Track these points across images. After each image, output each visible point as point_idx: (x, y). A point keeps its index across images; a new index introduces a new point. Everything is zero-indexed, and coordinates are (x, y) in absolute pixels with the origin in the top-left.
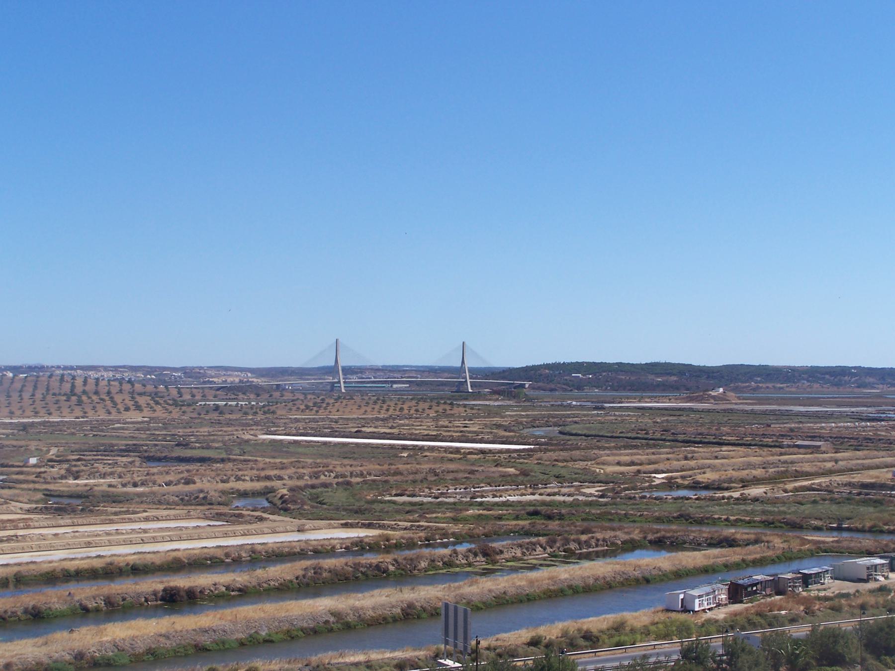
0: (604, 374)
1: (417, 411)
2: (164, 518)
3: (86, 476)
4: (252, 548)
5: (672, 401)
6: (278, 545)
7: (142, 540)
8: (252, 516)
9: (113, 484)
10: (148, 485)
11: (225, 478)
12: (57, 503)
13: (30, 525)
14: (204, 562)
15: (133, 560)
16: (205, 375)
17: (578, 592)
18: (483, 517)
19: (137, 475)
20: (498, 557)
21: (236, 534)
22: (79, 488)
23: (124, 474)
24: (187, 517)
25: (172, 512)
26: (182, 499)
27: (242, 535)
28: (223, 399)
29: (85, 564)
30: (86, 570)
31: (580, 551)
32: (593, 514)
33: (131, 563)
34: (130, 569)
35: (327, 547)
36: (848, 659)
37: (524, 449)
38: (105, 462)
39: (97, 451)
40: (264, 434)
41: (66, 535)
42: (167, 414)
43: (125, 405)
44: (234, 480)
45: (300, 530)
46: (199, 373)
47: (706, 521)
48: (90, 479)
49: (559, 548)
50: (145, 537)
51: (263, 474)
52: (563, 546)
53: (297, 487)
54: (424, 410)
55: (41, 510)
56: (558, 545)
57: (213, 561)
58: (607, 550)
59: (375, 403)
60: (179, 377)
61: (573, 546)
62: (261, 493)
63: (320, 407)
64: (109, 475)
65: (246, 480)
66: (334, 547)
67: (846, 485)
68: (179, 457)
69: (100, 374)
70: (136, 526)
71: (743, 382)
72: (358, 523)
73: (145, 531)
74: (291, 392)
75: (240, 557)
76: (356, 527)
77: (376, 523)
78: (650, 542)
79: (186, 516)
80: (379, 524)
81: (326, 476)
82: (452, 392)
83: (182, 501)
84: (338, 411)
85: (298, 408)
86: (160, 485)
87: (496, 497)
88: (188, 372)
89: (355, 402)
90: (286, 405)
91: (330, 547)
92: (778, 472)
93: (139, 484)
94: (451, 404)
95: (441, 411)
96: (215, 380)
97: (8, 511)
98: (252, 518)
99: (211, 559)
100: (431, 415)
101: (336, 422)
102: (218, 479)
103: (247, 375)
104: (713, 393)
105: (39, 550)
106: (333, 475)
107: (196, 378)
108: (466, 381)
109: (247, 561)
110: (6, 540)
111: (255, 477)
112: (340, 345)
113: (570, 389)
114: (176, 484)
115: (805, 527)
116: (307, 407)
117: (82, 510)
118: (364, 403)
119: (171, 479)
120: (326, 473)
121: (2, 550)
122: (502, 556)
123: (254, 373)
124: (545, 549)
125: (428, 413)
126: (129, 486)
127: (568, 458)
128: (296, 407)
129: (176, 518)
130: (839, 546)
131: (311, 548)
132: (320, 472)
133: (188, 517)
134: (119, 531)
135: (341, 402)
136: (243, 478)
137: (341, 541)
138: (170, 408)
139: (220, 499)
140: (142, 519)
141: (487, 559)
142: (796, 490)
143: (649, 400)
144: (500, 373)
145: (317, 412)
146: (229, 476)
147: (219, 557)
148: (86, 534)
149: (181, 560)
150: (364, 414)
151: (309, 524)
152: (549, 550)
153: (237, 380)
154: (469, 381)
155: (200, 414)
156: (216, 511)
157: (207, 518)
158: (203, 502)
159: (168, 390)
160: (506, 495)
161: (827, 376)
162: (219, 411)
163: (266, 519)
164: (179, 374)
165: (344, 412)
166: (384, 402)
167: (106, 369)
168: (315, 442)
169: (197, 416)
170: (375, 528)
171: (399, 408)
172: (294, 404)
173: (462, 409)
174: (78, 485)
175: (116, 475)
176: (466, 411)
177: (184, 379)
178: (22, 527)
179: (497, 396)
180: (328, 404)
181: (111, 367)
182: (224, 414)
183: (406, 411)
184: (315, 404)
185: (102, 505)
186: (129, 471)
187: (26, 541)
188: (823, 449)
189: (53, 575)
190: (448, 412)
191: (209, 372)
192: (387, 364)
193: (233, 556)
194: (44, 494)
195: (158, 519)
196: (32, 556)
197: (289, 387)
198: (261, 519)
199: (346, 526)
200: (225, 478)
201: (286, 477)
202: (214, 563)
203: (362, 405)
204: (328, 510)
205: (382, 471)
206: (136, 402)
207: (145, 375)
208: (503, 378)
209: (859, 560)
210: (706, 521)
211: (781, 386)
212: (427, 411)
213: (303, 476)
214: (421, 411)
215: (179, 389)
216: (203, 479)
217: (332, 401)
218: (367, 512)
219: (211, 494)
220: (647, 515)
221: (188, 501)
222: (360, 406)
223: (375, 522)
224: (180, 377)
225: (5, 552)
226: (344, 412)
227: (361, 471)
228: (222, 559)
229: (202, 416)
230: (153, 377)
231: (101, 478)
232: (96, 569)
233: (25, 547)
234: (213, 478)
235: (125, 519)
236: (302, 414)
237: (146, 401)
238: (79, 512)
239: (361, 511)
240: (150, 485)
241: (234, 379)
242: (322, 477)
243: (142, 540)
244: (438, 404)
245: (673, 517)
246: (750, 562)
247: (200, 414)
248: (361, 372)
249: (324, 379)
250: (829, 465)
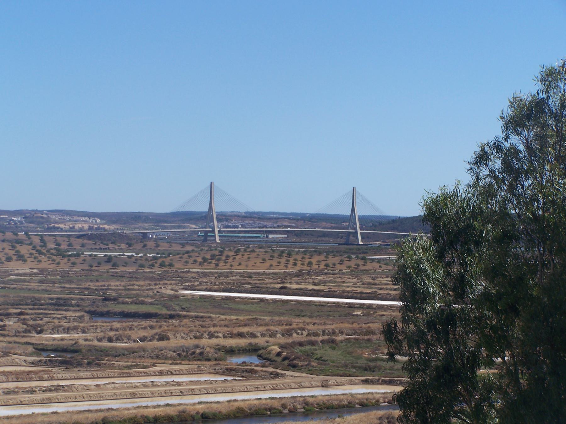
1: (327, 265)
2: (177, 372)
3: (49, 331)
4: (304, 400)
6: (327, 398)
7: (181, 392)
8: (266, 372)
9: (89, 338)
10: (123, 340)
11: (198, 334)
12: (60, 357)
13: (53, 377)
14: (265, 412)
15: (202, 408)
16: (48, 221)
19: (100, 330)
21: (267, 388)
22: (55, 342)
23: (88, 330)
24: (199, 372)
25: (177, 367)
26: (179, 355)
27: (272, 390)
28: (92, 249)
29: (160, 411)
30: (163, 418)
33: (201, 412)
34: (200, 418)
35: (372, 401)
38: (54, 316)
39: (33, 305)
41: (108, 386)
42: (54, 265)
43: (6, 254)
44: (208, 337)
45: (325, 386)
46: (42, 218)
48: (54, 333)
50: (184, 389)
51: (235, 331)
53: (288, 344)
54: (334, 265)
55: (45, 362)
57: (272, 411)
59: (280, 256)
60: (19, 221)
62: (246, 349)
63: (219, 260)
64: (72, 330)
65: (220, 337)
66: (378, 401)
68: (123, 312)
70: (148, 380)
72: (379, 379)
73: (179, 384)
74: (154, 241)
75: (295, 408)
76: (377, 384)
77: (397, 380)
79: (198, 371)
80: (400, 381)
81: (298, 334)
82: (339, 244)
83: (180, 357)
84: (240, 264)
85: (195, 261)
86: (134, 341)
89: (258, 255)
90: (181, 258)
91: (375, 401)
93: (114, 339)
94: (364, 259)
95: (353, 266)
96: (62, 226)
97: (13, 363)
98: (266, 374)
99: (270, 410)
100: (344, 271)
101: (250, 277)
102: (192, 335)
103: (96, 222)
105: (90, 399)
106: (305, 333)
107: (39, 223)
108: (356, 232)
109: (301, 412)
110: (54, 390)
111: (228, 334)
114: (150, 340)
116: (205, 260)
117: (89, 364)
118: (267, 256)
119: (146, 334)
120: (299, 331)
121: (58, 399)
123: (103, 219)
125: (341, 268)
126: (104, 340)
128: (193, 259)
129: (188, 373)
131: (357, 401)
132: (293, 329)
133: (200, 372)
134: (155, 383)
135: (243, 255)
136: (216, 334)
137: (382, 395)
138: (58, 259)
139: (216, 355)
140: (157, 373)
144: (389, 223)
145: (217, 265)
146: (202, 332)
147: (277, 408)
148: (125, 385)
149: (244, 410)
150: (269, 269)
151: (332, 380)
153: (86, 226)
154: (359, 232)
155: (91, 266)
156: (227, 366)
157: (216, 373)
158: (200, 357)
159: (29, 238)
162: (112, 263)
163: (283, 375)
164: (19, 219)
165: (247, 266)
166: (289, 255)
168: (250, 298)
169: (89, 268)
170: (397, 385)
171: (307, 262)
172: (190, 256)
173: (376, 265)
174: (54, 339)
175: (79, 330)
176: (380, 267)
177: (26, 224)
178: (47, 378)
180: (228, 257)
182: (118, 267)
183: (315, 267)
184: (213, 257)
185: (106, 359)
186: (93, 326)
187: (72, 391)
189: (135, 421)
191: (53, 217)
193: (289, 407)
194: (34, 348)
195: (172, 374)
196: (90, 405)
197: (152, 236)
198: (277, 376)
199: (366, 382)
200: (198, 334)
201: (259, 335)
202: (274, 413)
203: (267, 259)
204: (337, 367)
205: (354, 330)
206: (18, 252)
208: (393, 229)
212: (339, 267)
213: (276, 334)
214: (331, 266)
215: (42, 236)
216: (177, 335)
217: (231, 254)
218: (377, 369)
219: (207, 350)
221: (185, 357)
222: (264, 260)
223: (396, 379)
224: (21, 222)
225: (60, 401)
226: (247, 266)
227: (333, 330)
228: (280, 410)
229: (94, 268)
231: (64, 333)
232: (172, 417)
233: (77, 396)
234: (187, 335)
235: (141, 373)
236: (200, 267)
237: (28, 251)
238: (85, 366)
239: (370, 369)
240: (125, 341)
241: (83, 225)
242: (295, 335)
243: (181, 392)
244: (350, 258)
247: (91, 266)
248: (227, 220)
249: (184, 227)
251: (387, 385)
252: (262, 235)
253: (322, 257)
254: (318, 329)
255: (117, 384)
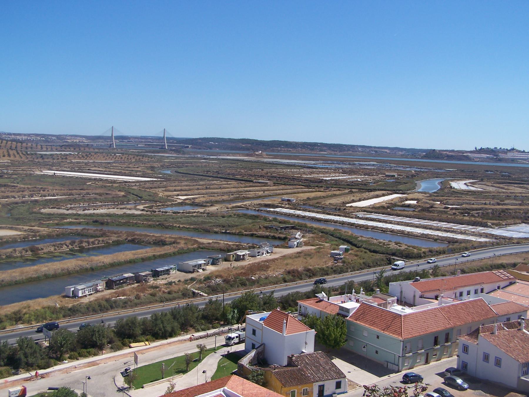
0: (223, 143)
5: (241, 156)
16: (65, 139)
17: (49, 278)
18: (72, 223)
20: (40, 252)
31: (88, 247)
32: (122, 223)
36: (98, 344)
37: (150, 180)
40: (48, 170)
47: (170, 227)
49: (76, 246)
52: (79, 245)
56: (76, 244)
58: (104, 246)
61: (84, 244)
67: (258, 205)
69: (21, 137)
71: (276, 148)
78: (129, 241)
84: (95, 158)
87: (95, 210)
88: (59, 137)
92: (235, 197)
96: (69, 141)
102: (40, 195)
104: (257, 153)
106: (40, 195)
108: (165, 144)
112: (113, 128)
113: (206, 148)
115: (211, 231)
116: (83, 156)
120: (37, 194)
122: (42, 251)
124: (68, 246)
127: (157, 187)
130: (209, 246)
132: (34, 194)
141: (33, 253)
142: (233, 207)
143: (231, 155)
145: (86, 158)
152: (70, 247)
153: (78, 141)
154: (166, 144)
160: (100, 209)
161: (309, 146)
167: (25, 135)
179: (172, 152)
181: (27, 134)
188: (269, 184)
190: (141, 159)
192: (143, 135)
206: (9, 153)
207: (40, 138)
209: (190, 262)
210: (170, 227)
211: (291, 150)
220: (146, 223)
222: (104, 156)
230: (44, 139)
245: (156, 225)
246: (158, 256)
247: (34, 159)
248: (129, 139)
250: (261, 193)
251: (10, 229)
252: (136, 145)
253: (127, 156)
254: (47, 194)
255: (364, 237)
